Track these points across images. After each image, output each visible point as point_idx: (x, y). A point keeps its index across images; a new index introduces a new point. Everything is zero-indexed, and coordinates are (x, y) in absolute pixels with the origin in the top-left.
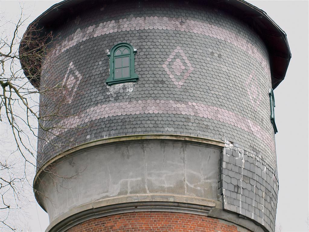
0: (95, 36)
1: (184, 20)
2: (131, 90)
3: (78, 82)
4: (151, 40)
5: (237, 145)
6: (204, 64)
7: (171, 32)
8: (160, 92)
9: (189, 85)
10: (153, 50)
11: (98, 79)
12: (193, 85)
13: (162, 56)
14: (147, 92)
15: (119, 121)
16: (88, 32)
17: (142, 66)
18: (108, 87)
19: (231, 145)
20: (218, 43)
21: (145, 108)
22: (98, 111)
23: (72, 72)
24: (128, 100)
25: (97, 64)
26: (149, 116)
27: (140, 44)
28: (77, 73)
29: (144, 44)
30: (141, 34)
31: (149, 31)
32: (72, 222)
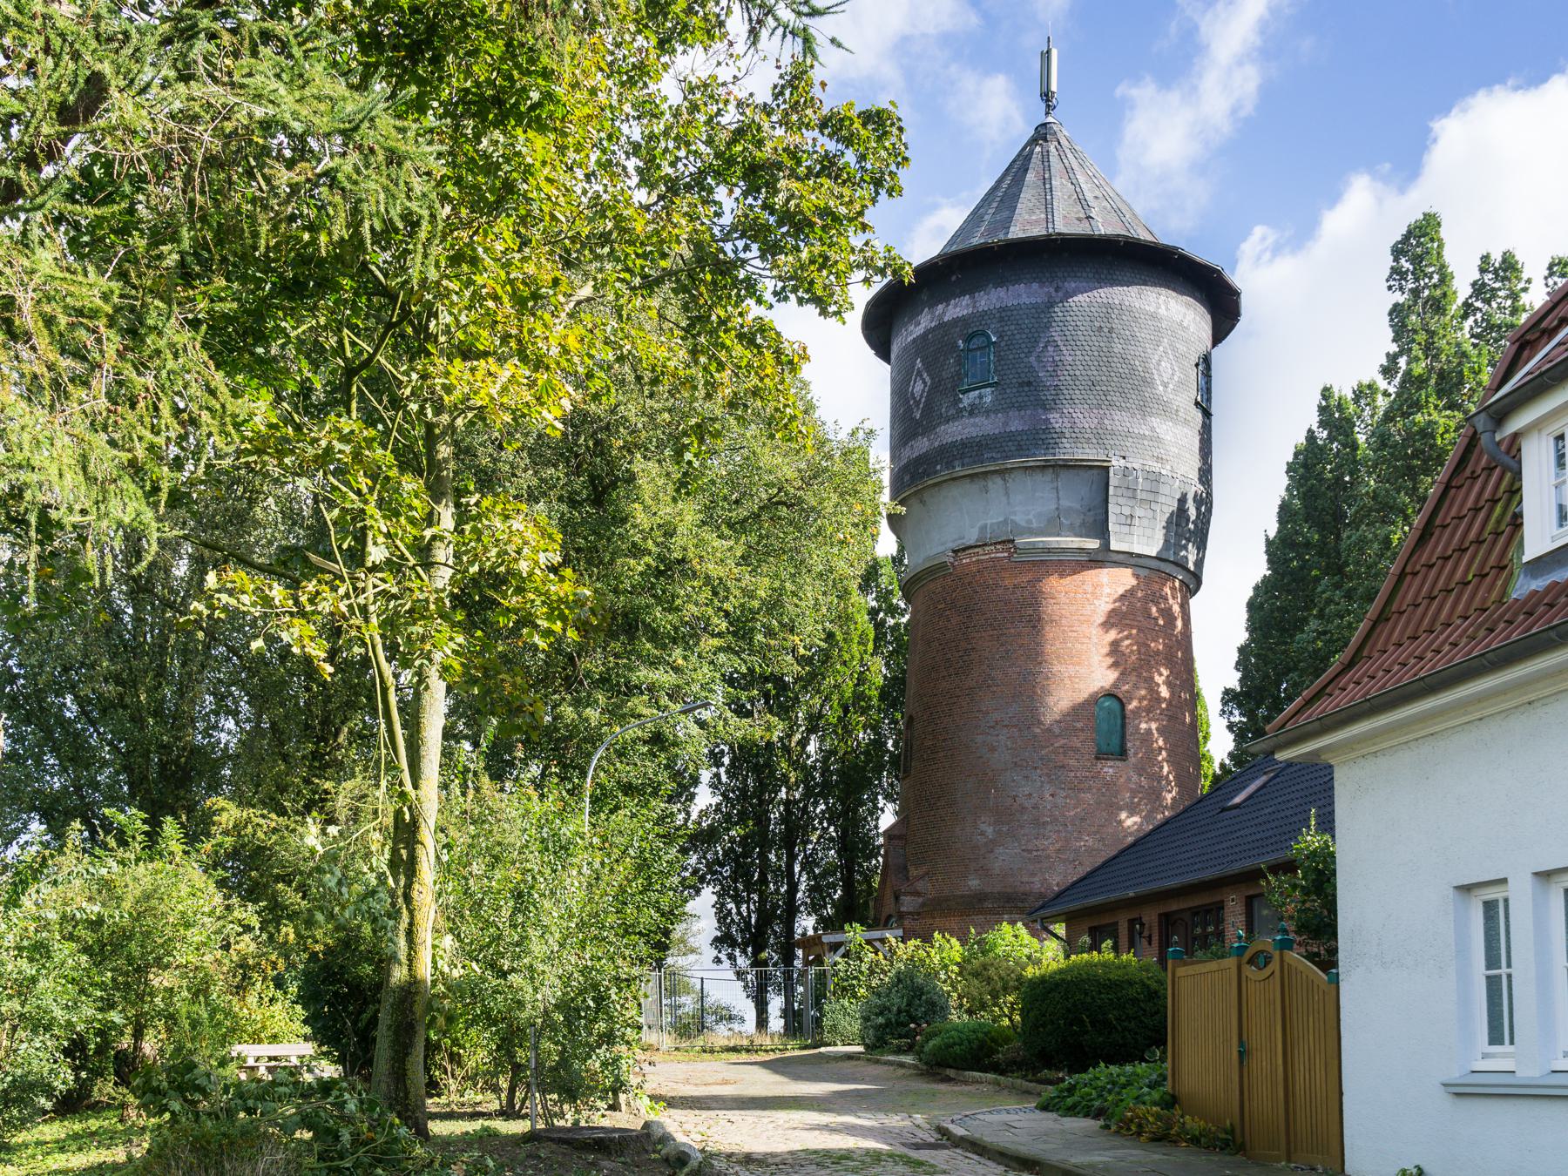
2: (988, 399)
21: (1006, 424)
23: (919, 374)
32: (1500, 583)
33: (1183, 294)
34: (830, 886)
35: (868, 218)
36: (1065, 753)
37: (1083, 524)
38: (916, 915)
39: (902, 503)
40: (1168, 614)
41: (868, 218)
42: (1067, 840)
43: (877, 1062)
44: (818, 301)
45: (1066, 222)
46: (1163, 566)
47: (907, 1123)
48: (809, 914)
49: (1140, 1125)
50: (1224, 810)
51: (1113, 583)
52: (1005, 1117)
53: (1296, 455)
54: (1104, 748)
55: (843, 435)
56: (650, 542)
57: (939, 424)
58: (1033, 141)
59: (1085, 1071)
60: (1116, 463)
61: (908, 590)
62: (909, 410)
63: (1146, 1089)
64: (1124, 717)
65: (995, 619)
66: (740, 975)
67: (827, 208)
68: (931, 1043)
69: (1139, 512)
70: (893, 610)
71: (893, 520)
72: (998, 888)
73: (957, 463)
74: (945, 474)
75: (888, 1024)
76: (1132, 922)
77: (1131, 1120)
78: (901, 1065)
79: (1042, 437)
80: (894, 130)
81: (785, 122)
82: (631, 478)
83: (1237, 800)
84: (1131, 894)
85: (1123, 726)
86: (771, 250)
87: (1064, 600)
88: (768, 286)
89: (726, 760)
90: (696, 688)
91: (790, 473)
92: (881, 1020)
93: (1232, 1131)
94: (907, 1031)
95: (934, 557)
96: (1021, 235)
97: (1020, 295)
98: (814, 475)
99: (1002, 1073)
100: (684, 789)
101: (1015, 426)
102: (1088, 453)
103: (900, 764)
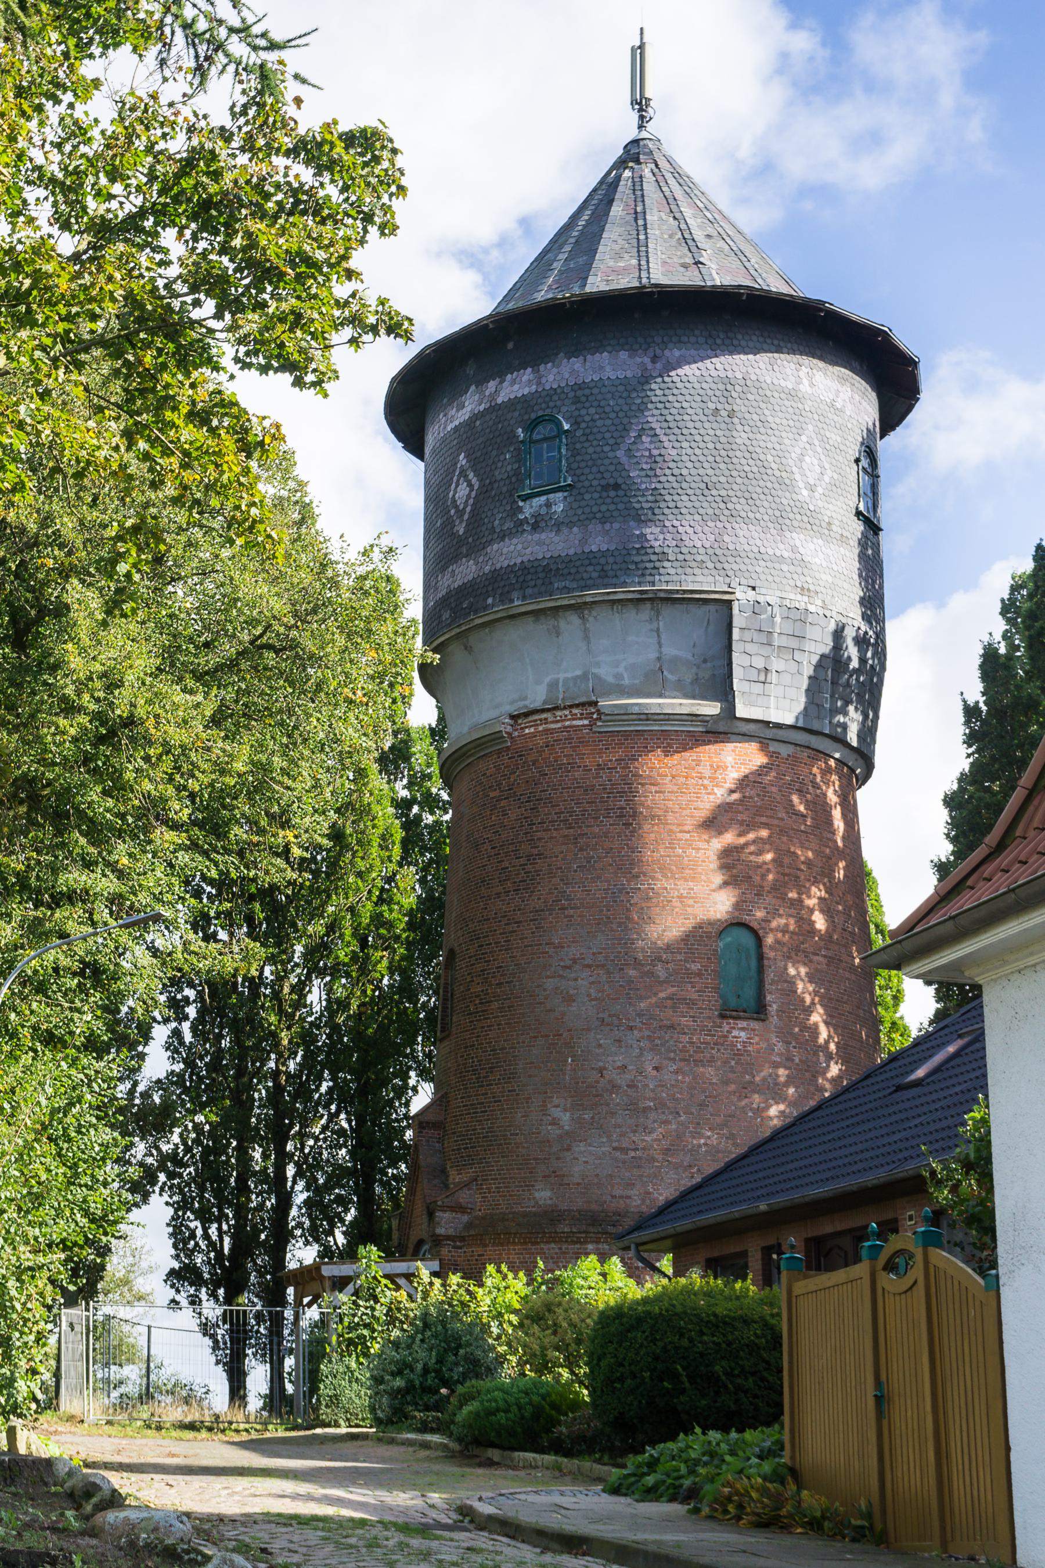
0: (499, 400)
1: (658, 352)
2: (559, 508)
3: (473, 494)
4: (595, 404)
5: (763, 591)
6: (698, 438)
7: (634, 382)
8: (612, 507)
9: (667, 485)
10: (599, 423)
11: (505, 489)
12: (675, 485)
13: (615, 434)
14: (587, 510)
15: (540, 569)
16: (487, 393)
17: (578, 458)
18: (521, 504)
19: (751, 593)
20: (729, 387)
21: (584, 541)
22: (505, 550)
23: (463, 473)
24: (555, 529)
25: (502, 458)
26: (591, 556)
27: (576, 413)
28: (471, 475)
29: (583, 412)
30: (579, 393)
31: (592, 385)
33: (834, 363)
34: (341, 1200)
35: (352, 264)
36: (674, 1007)
37: (696, 680)
38: (459, 1240)
39: (435, 651)
40: (820, 809)
41: (352, 264)
42: (679, 1136)
43: (392, 1441)
44: (288, 366)
45: (666, 269)
46: (815, 742)
47: (418, 1502)
48: (307, 1243)
49: (740, 1507)
50: (899, 1088)
51: (737, 760)
52: (557, 1499)
53: (1014, 589)
54: (733, 1002)
55: (352, 555)
56: (86, 697)
57: (490, 542)
58: (621, 164)
59: (673, 1438)
60: (742, 596)
61: (451, 769)
62: (449, 523)
63: (754, 1460)
64: (761, 957)
65: (571, 812)
66: (206, 1329)
67: (300, 253)
68: (466, 1410)
69: (776, 664)
70: (431, 802)
71: (429, 676)
72: (579, 1204)
73: (515, 595)
74: (500, 610)
75: (410, 1388)
76: (767, 1251)
77: (729, 1499)
78: (426, 1445)
79: (633, 559)
80: (386, 154)
81: (249, 146)
82: (61, 610)
83: (920, 1073)
84: (763, 1207)
85: (761, 970)
86: (227, 305)
87: (670, 787)
88: (226, 351)
89: (192, 1011)
90: (143, 898)
91: (279, 606)
92: (399, 1383)
93: (869, 1516)
94: (434, 1394)
95: (485, 725)
96: (604, 287)
97: (605, 366)
98: (309, 609)
99: (568, 1454)
100: (125, 1037)
101: (598, 543)
102: (702, 581)
103: (438, 1025)
